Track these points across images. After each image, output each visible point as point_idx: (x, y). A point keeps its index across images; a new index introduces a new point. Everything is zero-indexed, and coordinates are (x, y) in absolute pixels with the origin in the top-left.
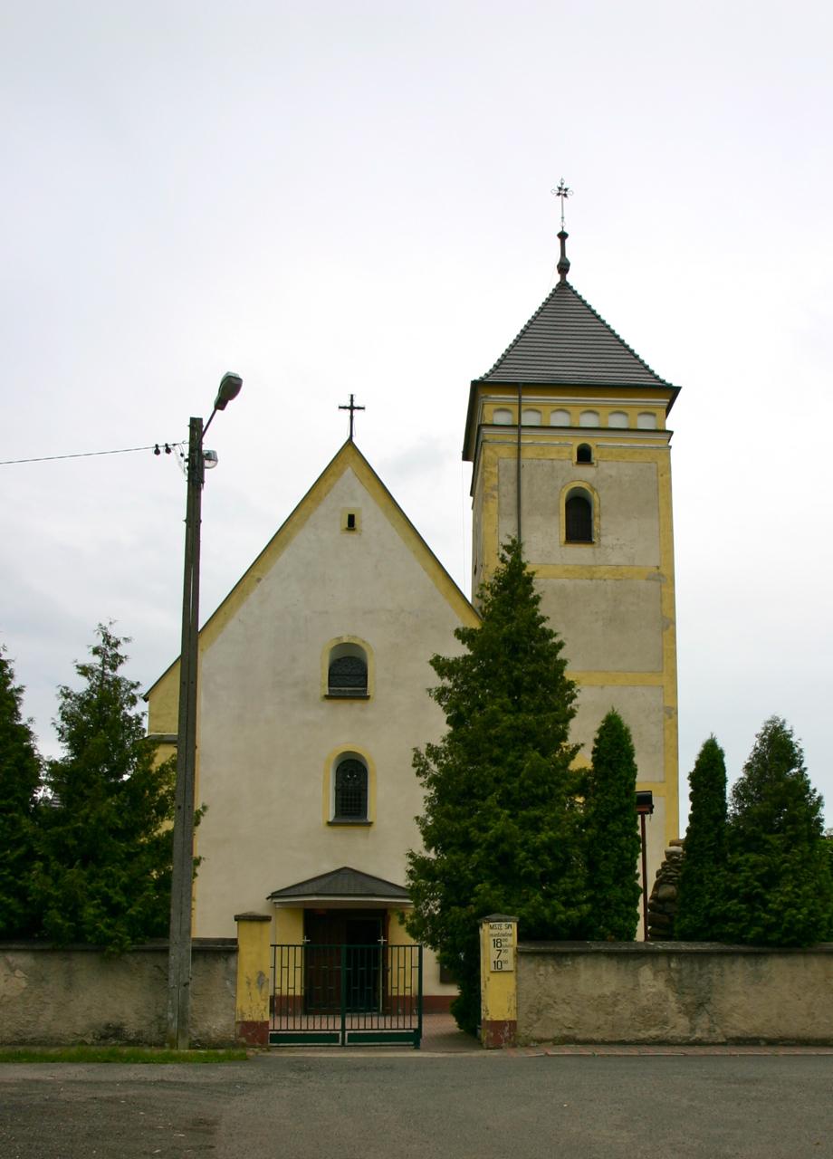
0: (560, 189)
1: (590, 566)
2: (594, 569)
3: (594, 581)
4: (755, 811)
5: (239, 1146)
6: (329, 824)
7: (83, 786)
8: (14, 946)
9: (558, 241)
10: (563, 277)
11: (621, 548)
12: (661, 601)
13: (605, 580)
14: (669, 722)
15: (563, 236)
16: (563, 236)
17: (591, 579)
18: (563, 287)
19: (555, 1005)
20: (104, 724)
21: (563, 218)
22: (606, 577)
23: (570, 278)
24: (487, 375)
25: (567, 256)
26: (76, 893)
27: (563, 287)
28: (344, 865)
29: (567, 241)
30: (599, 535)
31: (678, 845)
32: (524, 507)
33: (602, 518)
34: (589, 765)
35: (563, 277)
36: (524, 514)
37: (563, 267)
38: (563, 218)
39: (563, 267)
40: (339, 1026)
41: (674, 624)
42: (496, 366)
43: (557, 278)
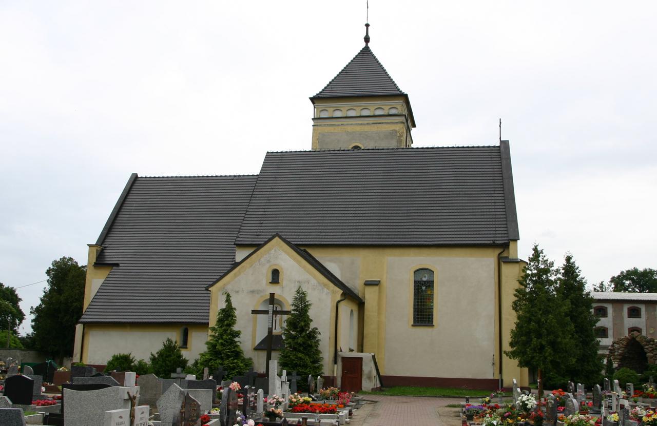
4: (569, 327)
5: (67, 286)
6: (270, 283)
9: (365, 27)
10: (367, 45)
15: (367, 25)
16: (367, 25)
20: (71, 380)
23: (369, 45)
24: (320, 93)
25: (369, 34)
26: (319, 133)
28: (336, 302)
29: (369, 28)
34: (30, 331)
35: (367, 45)
37: (367, 39)
39: (367, 39)
40: (202, 368)
42: (323, 90)
43: (364, 45)
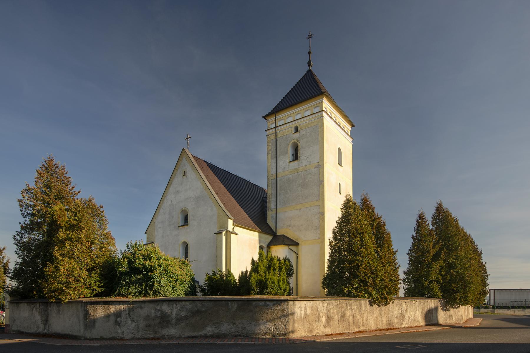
0: (311, 37)
1: (297, 168)
2: (298, 169)
3: (298, 173)
7: (45, 166)
8: (23, 302)
11: (307, 159)
12: (319, 175)
13: (301, 172)
14: (322, 217)
15: (309, 53)
16: (309, 53)
17: (297, 173)
18: (310, 71)
19: (75, 193)
21: (310, 46)
22: (302, 171)
27: (310, 71)
30: (300, 157)
31: (435, 302)
32: (278, 154)
33: (301, 150)
36: (278, 156)
38: (310, 46)
39: (309, 64)
41: (324, 182)
